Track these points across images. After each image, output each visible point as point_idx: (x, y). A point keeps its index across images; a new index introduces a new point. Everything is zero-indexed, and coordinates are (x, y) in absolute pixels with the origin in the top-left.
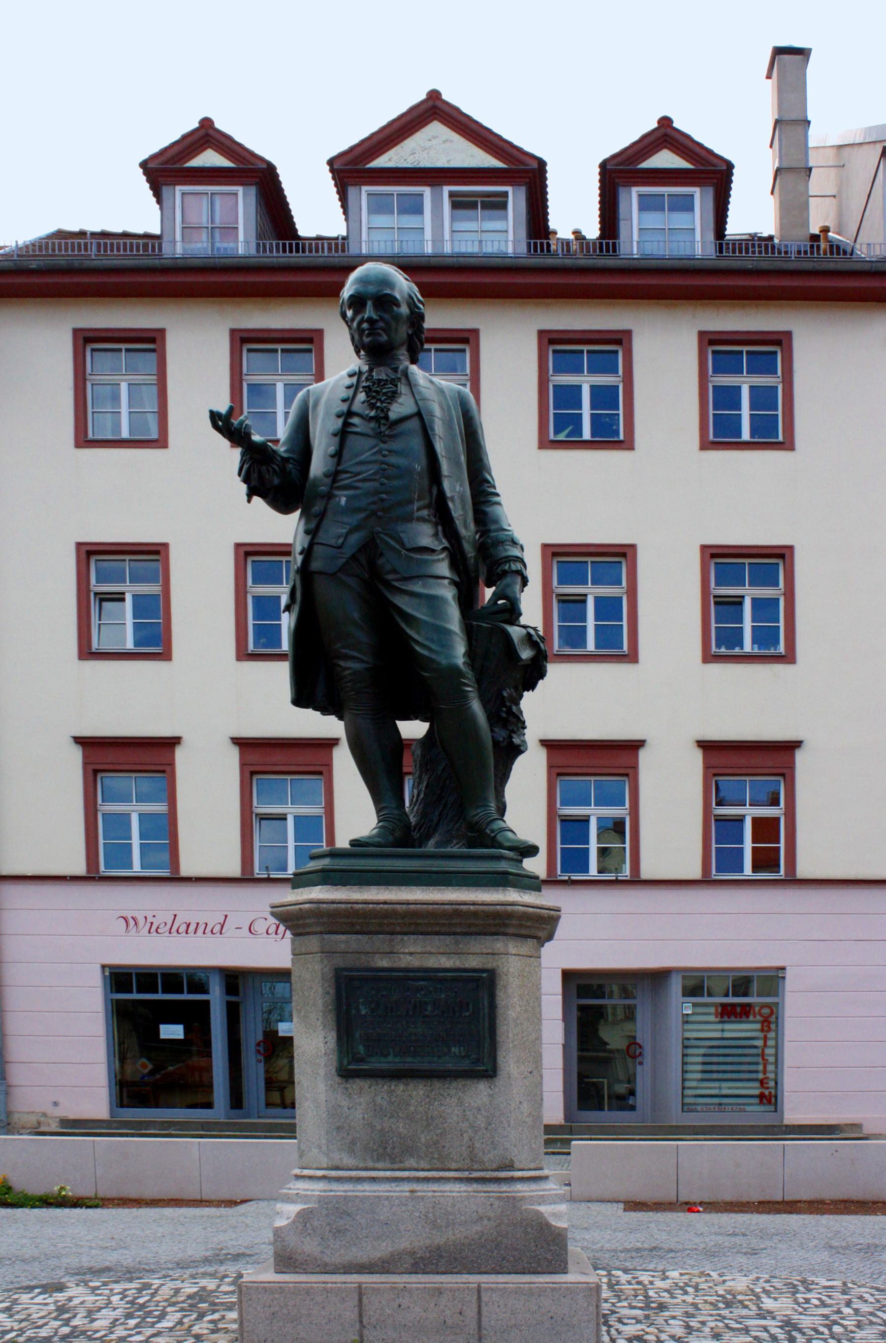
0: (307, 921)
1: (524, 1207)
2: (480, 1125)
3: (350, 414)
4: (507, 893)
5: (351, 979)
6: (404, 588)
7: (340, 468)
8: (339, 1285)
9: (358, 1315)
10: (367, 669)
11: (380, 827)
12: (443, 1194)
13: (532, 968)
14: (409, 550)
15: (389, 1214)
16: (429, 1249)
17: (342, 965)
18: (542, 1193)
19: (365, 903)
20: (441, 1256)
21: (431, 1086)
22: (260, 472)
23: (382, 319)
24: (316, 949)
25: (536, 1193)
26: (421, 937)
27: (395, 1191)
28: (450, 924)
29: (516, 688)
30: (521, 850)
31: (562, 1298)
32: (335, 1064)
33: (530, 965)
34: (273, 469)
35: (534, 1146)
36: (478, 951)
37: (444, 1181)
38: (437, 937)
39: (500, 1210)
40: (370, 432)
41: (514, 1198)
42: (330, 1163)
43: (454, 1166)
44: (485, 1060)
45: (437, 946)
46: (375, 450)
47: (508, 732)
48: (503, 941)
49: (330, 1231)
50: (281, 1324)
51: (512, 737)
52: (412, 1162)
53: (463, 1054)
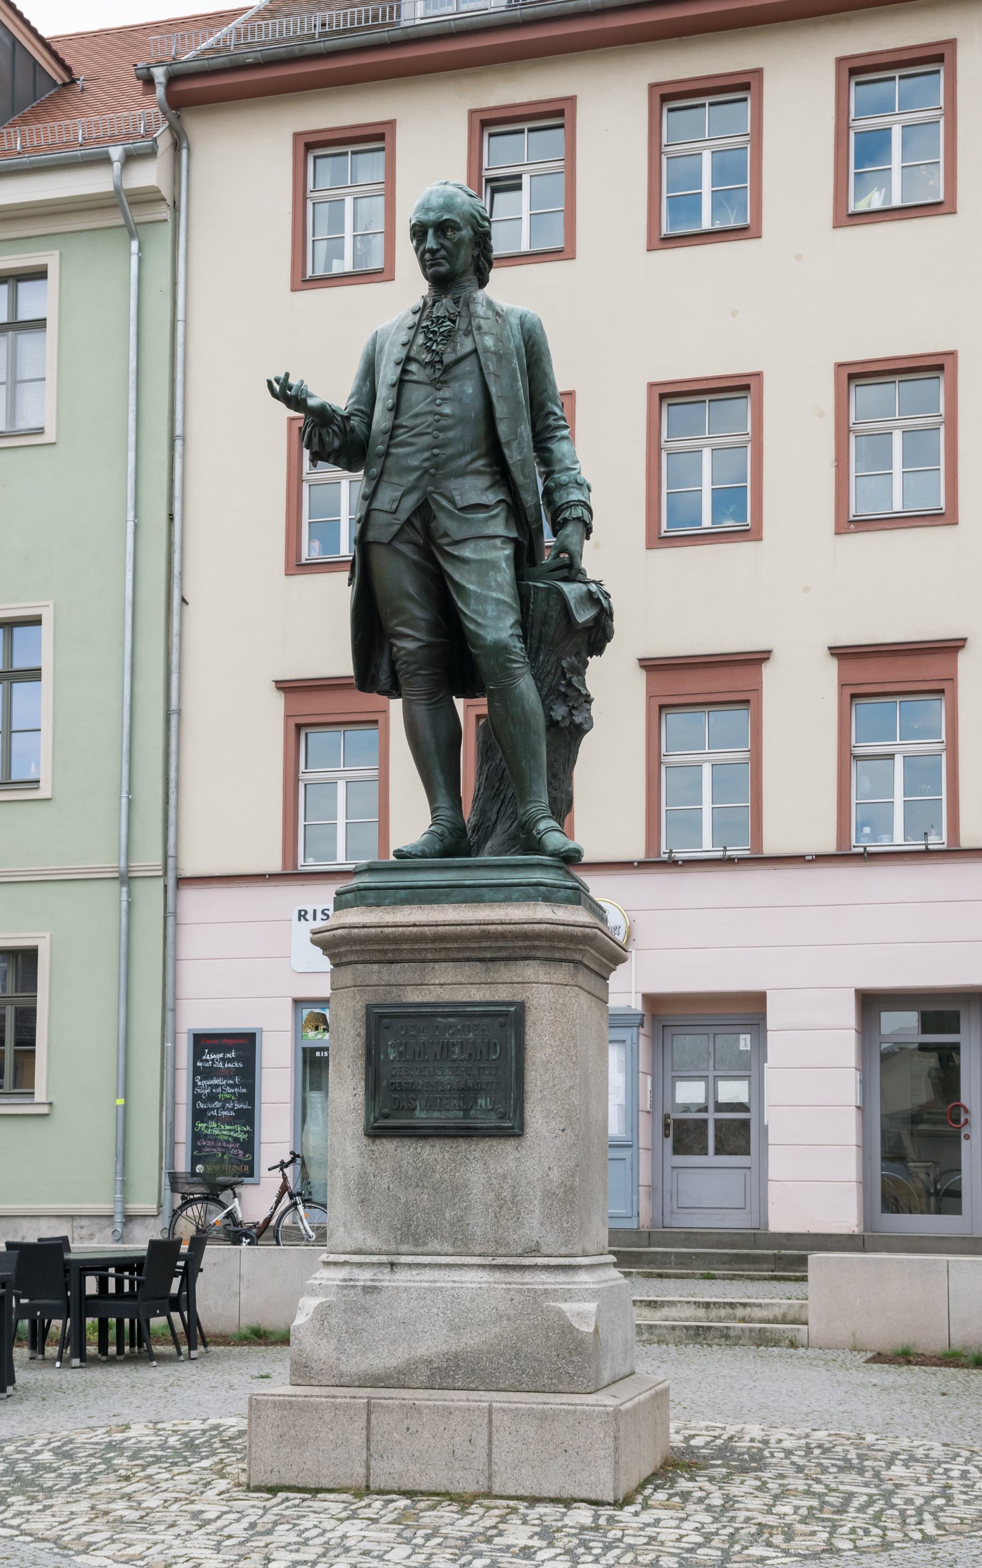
0: (342, 949)
1: (545, 1305)
2: (505, 1196)
3: (409, 359)
4: (539, 909)
5: (382, 1016)
6: (456, 553)
7: (398, 422)
8: (348, 1400)
9: (365, 1441)
10: (420, 648)
11: (431, 832)
12: (463, 1285)
13: (567, 999)
14: (462, 509)
15: (407, 1310)
16: (446, 1356)
17: (374, 1001)
18: (569, 1287)
19: (395, 926)
20: (458, 1366)
21: (457, 1147)
22: (320, 434)
23: (443, 246)
24: (350, 983)
25: (562, 1286)
26: (452, 963)
27: (414, 1281)
28: (480, 948)
29: (577, 655)
30: (562, 855)
31: (577, 1424)
32: (363, 1120)
33: (565, 996)
34: (333, 431)
35: (565, 1225)
36: (508, 980)
37: (466, 1268)
38: (468, 964)
39: (520, 1306)
40: (426, 379)
41: (535, 1291)
42: (353, 1246)
43: (478, 1249)
44: (511, 1115)
45: (467, 976)
46: (429, 399)
47: (566, 709)
48: (534, 967)
49: (347, 1332)
50: (288, 1450)
51: (573, 715)
52: (435, 1245)
53: (490, 1107)
